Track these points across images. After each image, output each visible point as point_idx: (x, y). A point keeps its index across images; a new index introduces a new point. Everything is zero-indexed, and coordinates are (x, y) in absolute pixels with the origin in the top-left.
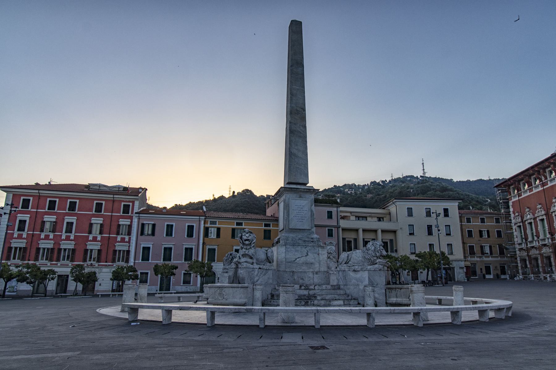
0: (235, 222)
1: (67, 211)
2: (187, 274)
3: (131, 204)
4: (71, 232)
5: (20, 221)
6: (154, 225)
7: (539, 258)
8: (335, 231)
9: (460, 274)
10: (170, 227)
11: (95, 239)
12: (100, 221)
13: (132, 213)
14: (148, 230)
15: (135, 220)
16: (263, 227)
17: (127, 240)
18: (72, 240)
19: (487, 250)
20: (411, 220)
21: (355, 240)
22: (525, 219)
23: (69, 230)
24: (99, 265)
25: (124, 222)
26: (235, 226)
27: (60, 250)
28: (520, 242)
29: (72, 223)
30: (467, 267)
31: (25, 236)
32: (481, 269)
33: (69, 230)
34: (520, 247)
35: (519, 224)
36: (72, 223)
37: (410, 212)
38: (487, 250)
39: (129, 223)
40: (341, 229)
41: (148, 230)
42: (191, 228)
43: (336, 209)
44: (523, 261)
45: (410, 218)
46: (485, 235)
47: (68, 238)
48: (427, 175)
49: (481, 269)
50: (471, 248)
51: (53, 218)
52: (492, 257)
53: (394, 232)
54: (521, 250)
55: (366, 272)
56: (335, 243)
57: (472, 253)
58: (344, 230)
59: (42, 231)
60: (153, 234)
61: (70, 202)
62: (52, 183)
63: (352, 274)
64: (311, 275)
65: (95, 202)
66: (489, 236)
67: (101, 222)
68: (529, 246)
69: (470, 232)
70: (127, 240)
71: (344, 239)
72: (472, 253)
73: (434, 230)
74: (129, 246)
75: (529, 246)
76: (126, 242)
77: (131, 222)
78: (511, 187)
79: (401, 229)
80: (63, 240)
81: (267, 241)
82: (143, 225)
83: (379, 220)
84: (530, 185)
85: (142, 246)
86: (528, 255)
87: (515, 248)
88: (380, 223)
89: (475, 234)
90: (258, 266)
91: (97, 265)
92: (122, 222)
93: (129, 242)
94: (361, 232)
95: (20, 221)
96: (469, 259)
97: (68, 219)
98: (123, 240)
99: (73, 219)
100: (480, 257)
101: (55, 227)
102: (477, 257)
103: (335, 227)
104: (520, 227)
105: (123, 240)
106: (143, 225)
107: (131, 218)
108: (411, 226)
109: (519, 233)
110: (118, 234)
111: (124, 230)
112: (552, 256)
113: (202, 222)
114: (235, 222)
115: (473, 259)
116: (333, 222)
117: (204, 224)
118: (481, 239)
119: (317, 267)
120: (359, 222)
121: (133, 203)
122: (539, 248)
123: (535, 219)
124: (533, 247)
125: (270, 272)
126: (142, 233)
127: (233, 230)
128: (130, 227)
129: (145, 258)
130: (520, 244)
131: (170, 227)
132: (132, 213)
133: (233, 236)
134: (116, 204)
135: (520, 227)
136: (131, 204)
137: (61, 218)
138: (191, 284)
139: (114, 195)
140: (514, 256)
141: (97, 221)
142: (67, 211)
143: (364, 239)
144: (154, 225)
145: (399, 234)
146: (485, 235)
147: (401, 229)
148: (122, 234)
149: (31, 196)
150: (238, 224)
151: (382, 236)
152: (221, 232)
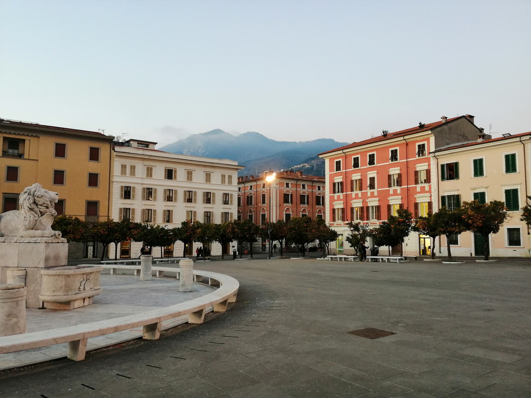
5: (370, 178)
15: (433, 162)
23: (372, 186)
25: (421, 167)
27: (368, 208)
31: (376, 194)
39: (426, 168)
47: (372, 195)
48: (84, 214)
70: (427, 189)
73: (102, 180)
74: (431, 196)
76: (427, 192)
77: (429, 165)
91: (343, 224)
93: (430, 192)
95: (370, 178)
98: (423, 190)
107: (428, 160)
109: (217, 170)
111: (423, 177)
121: (428, 140)
128: (428, 172)
134: (410, 146)
139: (343, 150)
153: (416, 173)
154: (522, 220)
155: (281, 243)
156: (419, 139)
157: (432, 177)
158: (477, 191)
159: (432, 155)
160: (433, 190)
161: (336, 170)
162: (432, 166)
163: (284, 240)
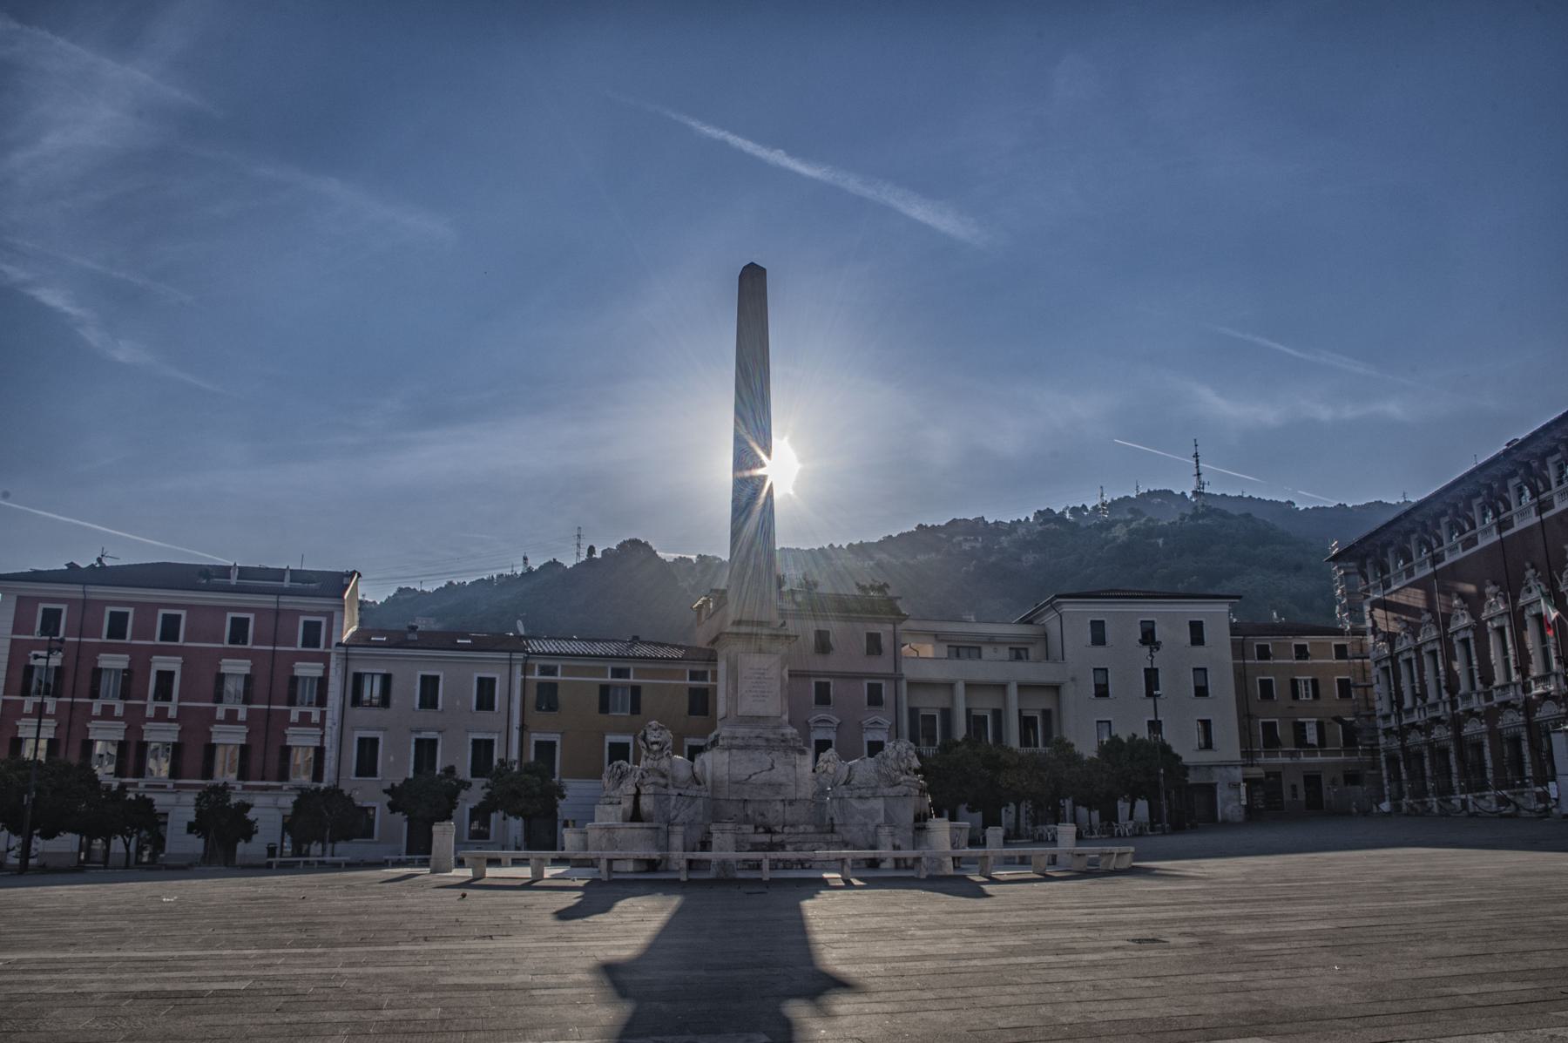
0: (610, 666)
1: (226, 644)
2: (481, 814)
3: (324, 620)
4: (169, 699)
5: (159, 673)
6: (387, 679)
7: (1426, 753)
8: (887, 692)
9: (1231, 803)
10: (430, 684)
11: (231, 717)
12: (243, 667)
13: (328, 645)
14: (372, 690)
16: (688, 682)
17: (315, 718)
18: (171, 721)
19: (1312, 737)
20: (1100, 656)
21: (997, 714)
22: (1398, 649)
23: (164, 692)
24: (244, 788)
25: (307, 670)
26: (609, 679)
28: (1386, 710)
29: (171, 674)
30: (1251, 783)
31: (172, 713)
32: (1294, 787)
33: (164, 692)
34: (1388, 725)
35: (1384, 664)
36: (171, 674)
37: (1098, 634)
38: (1312, 737)
39: (319, 673)
40: (904, 685)
41: (372, 690)
42: (486, 686)
43: (890, 627)
44: (1392, 760)
45: (1099, 649)
46: (1305, 695)
47: (161, 715)
49: (1294, 787)
50: (1269, 728)
51: (120, 662)
52: (1324, 753)
53: (1056, 689)
54: (1388, 732)
55: (881, 801)
56: (887, 723)
57: (1272, 741)
58: (914, 685)
59: (219, 699)
60: (385, 701)
61: (45, 610)
62: (108, 562)
63: (854, 802)
64: (779, 807)
65: (230, 615)
66: (1316, 695)
67: (247, 670)
68: (1404, 722)
69: (1266, 686)
70: (315, 718)
71: (913, 712)
72: (1272, 741)
74: (322, 737)
75: (1404, 722)
77: (327, 670)
78: (1369, 561)
79: (1073, 679)
80: (150, 720)
81: (697, 720)
82: (358, 678)
83: (1018, 657)
84: (1408, 559)
85: (358, 734)
86: (1403, 748)
87: (1376, 729)
88: (1019, 665)
89: (1280, 691)
90: (675, 792)
92: (107, 661)
93: (322, 725)
94: (1013, 691)
95: (159, 673)
96: (1262, 759)
97: (160, 663)
98: (305, 719)
99: (173, 664)
100: (1292, 754)
101: (129, 684)
102: (1286, 754)
103: (886, 677)
104: (1385, 669)
105: (305, 719)
106: (358, 678)
107: (325, 658)
108: (1201, 672)
110: (94, 694)
111: (307, 692)
112: (1452, 748)
113: (518, 670)
114: (610, 666)
115: (1273, 760)
116: (882, 665)
117: (524, 673)
118: (1295, 704)
119: (790, 792)
120: (956, 662)
122: (1426, 729)
123: (1418, 649)
124: (1413, 725)
125: (700, 802)
126: (357, 700)
127: (605, 689)
128: (323, 682)
129: (367, 766)
130: (1386, 717)
131: (430, 684)
132: (328, 645)
133: (604, 707)
135: (1385, 669)
136: (324, 620)
137: (142, 658)
138: (376, 838)
140: (1374, 751)
141: (235, 668)
142: (226, 644)
143: (968, 711)
144: (387, 679)
145: (1068, 693)
146: (1305, 695)
147: (1073, 679)
148: (302, 704)
149: (129, 604)
150: (618, 673)
151: (966, 699)
152: (643, 697)
153: (97, 672)
154: (166, 815)
155: (127, 846)
156: (307, 608)
157: (331, 696)
158: (423, 735)
159: (342, 650)
160: (328, 723)
161: (231, 641)
162: (332, 672)
163: (134, 840)
